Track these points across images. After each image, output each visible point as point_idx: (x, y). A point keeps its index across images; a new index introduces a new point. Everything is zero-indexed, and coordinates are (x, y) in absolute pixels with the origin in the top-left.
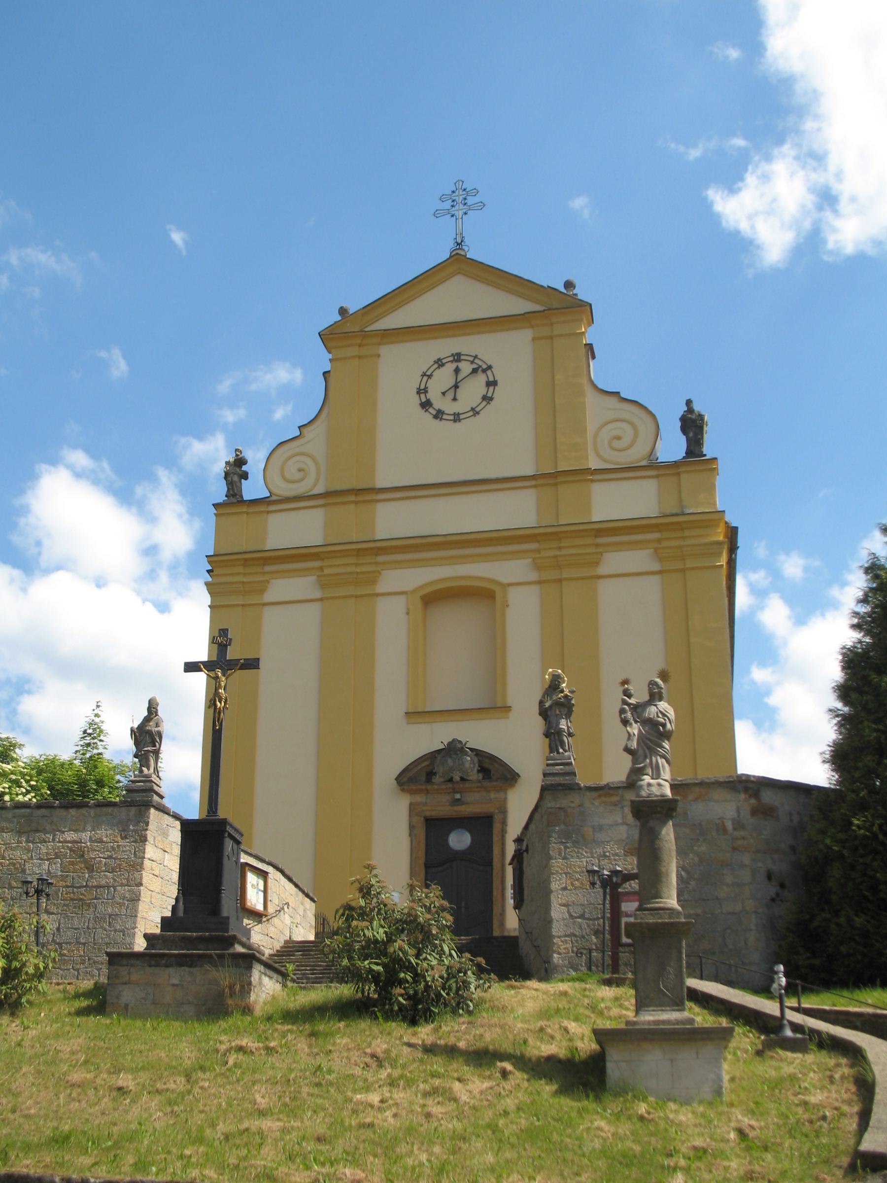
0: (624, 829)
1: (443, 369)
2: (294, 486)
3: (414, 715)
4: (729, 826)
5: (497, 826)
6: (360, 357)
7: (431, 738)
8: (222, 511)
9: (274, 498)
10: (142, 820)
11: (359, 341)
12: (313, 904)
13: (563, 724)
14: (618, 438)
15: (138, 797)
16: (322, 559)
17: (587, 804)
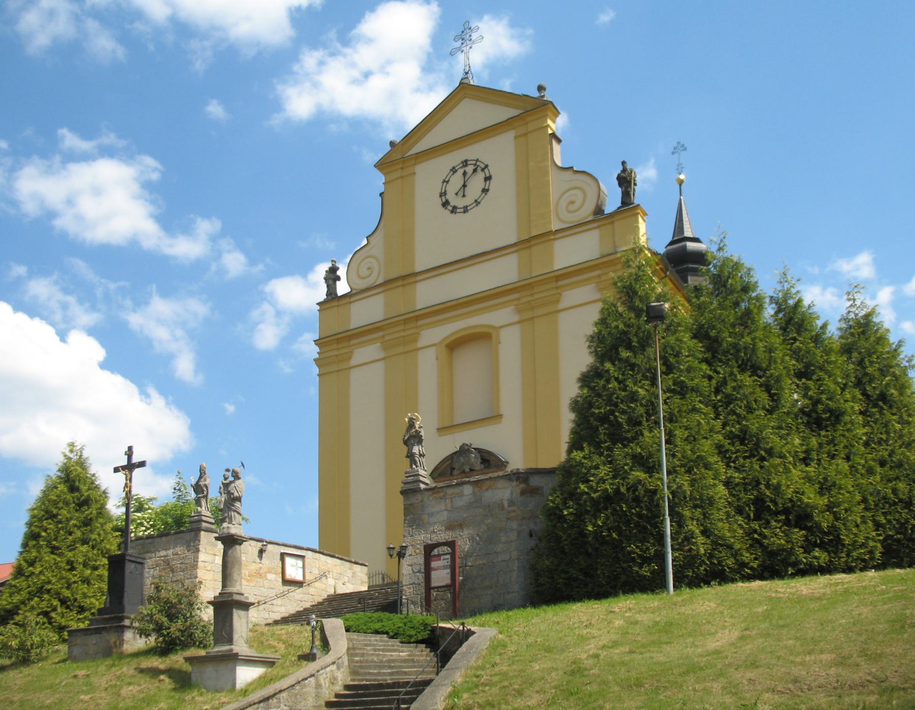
0: (445, 513)
1: (456, 174)
2: (365, 281)
3: (442, 430)
4: (506, 504)
6: (402, 177)
7: (450, 444)
8: (324, 307)
9: (354, 292)
10: (197, 538)
11: (400, 166)
12: (365, 569)
13: (416, 450)
14: (573, 202)
15: (195, 526)
16: (383, 330)
17: (425, 499)
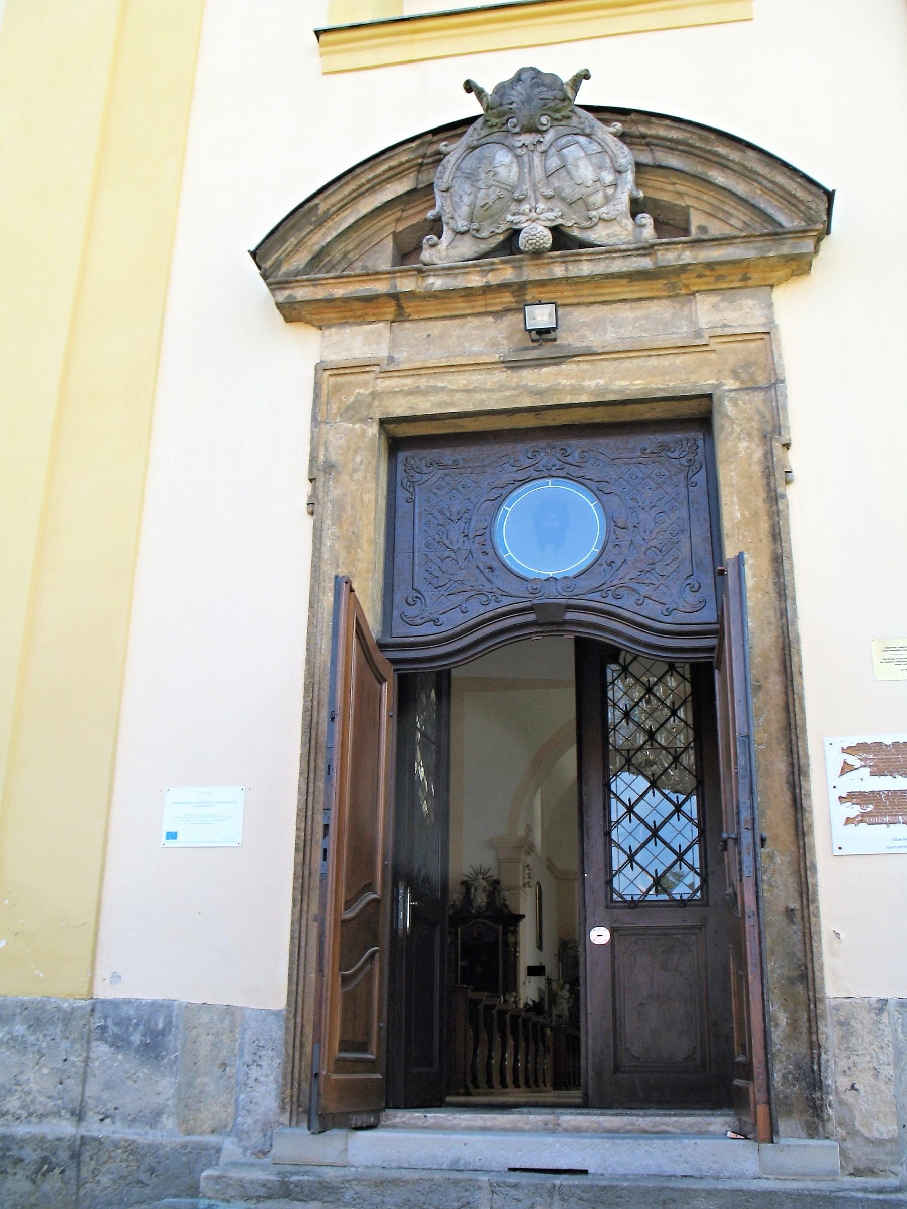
5: (736, 453)
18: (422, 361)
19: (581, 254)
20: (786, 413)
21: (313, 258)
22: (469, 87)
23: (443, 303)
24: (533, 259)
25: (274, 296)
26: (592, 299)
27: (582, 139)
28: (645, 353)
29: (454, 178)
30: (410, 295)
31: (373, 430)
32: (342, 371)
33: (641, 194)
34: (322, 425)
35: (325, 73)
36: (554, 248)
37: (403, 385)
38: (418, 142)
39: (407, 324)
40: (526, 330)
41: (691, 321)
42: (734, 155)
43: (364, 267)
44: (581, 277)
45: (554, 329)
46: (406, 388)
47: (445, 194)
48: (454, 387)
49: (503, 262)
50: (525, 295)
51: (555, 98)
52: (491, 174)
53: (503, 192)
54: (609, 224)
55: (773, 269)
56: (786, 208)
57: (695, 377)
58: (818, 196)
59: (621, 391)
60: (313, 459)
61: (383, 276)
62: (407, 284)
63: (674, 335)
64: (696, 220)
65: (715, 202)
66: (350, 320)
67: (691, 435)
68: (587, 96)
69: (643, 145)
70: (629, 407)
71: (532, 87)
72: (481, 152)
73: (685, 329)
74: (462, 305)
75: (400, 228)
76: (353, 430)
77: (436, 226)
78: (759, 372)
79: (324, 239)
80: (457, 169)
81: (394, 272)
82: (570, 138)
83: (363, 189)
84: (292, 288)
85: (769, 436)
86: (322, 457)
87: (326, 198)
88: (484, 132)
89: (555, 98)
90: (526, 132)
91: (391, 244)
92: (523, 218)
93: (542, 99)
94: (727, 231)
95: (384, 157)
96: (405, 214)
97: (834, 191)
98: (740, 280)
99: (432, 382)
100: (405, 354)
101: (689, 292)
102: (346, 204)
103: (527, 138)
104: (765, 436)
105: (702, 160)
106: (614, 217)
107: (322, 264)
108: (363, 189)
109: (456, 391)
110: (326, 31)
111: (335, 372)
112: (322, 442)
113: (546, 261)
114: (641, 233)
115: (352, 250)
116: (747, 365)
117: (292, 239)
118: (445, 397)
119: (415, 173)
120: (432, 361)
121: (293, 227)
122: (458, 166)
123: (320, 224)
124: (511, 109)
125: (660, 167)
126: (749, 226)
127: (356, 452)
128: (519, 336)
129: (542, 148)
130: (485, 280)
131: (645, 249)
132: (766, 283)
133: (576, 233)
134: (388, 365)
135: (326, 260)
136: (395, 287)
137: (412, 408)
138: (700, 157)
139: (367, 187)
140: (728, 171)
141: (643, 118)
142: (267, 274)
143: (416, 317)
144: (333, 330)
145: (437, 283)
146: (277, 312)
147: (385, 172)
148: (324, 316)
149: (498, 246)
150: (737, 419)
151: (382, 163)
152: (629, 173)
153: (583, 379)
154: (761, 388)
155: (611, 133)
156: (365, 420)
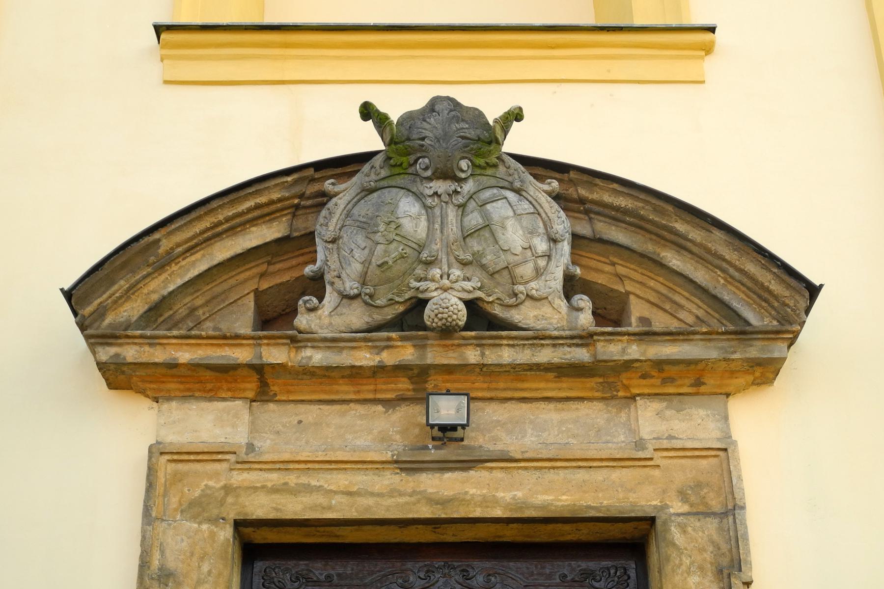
18: (291, 453)
19: (501, 338)
20: (747, 544)
21: (150, 310)
22: (367, 112)
23: (321, 384)
24: (441, 338)
25: (94, 353)
26: (509, 394)
27: (510, 195)
28: (574, 464)
29: (343, 226)
30: (281, 368)
31: (226, 533)
32: (186, 457)
33: (578, 271)
34: (157, 523)
35: (166, 82)
36: (467, 327)
37: (268, 480)
38: (295, 176)
39: (271, 406)
40: (428, 424)
41: (630, 430)
42: (696, 234)
43: (215, 329)
44: (501, 365)
45: (463, 427)
46: (269, 485)
47: (330, 246)
48: (332, 487)
49: (402, 339)
50: (426, 382)
51: (479, 139)
52: (393, 226)
53: (408, 250)
54: (538, 304)
55: (733, 373)
56: (755, 302)
57: (634, 495)
58: (799, 292)
59: (542, 507)
60: (144, 564)
61: (244, 342)
62: (276, 355)
63: (610, 445)
64: (637, 310)
65: (664, 290)
66: (197, 394)
67: (621, 563)
68: (517, 142)
69: (580, 212)
70: (550, 527)
71: (450, 121)
72: (379, 197)
73: (622, 438)
74: (345, 388)
75: (265, 285)
76: (197, 532)
77: (316, 285)
78: (712, 495)
79: (165, 287)
80: (347, 216)
81: (260, 338)
82: (495, 191)
83: (220, 229)
84: (120, 345)
85: (726, 572)
86: (156, 563)
87: (170, 234)
88: (384, 173)
89: (479, 139)
90: (438, 178)
91: (252, 304)
92: (432, 286)
93: (463, 138)
94: (674, 325)
95: (250, 190)
96: (272, 268)
97: (821, 286)
98: (692, 385)
99: (304, 480)
100: (268, 441)
101: (628, 395)
102: (197, 245)
103: (441, 186)
104: (720, 571)
105: (654, 237)
106: (545, 295)
107: (162, 319)
108: (220, 229)
109: (335, 492)
110: (170, 28)
111: (175, 457)
112: (157, 544)
113: (456, 342)
114: (577, 318)
115: (201, 306)
116: (699, 485)
117: (122, 282)
118: (321, 499)
119: (289, 217)
120: (305, 454)
121: (124, 266)
122: (349, 212)
123: (161, 267)
124: (422, 146)
125: (601, 241)
126: (703, 321)
127: (202, 559)
128: (417, 431)
129: (460, 200)
130: (377, 359)
131: (581, 337)
132: (723, 391)
133: (497, 311)
134: (247, 454)
135: (166, 315)
136: (261, 357)
137: (277, 510)
138: (650, 232)
139: (225, 226)
140: (683, 252)
141: (585, 178)
142: (87, 323)
143: (284, 398)
144: (174, 404)
145: (317, 357)
146: (98, 374)
147: (249, 210)
148: (162, 386)
149: (396, 317)
150: (686, 549)
151: (246, 198)
152: (566, 243)
153: (497, 489)
154: (714, 514)
155: (545, 192)
156: (214, 521)
